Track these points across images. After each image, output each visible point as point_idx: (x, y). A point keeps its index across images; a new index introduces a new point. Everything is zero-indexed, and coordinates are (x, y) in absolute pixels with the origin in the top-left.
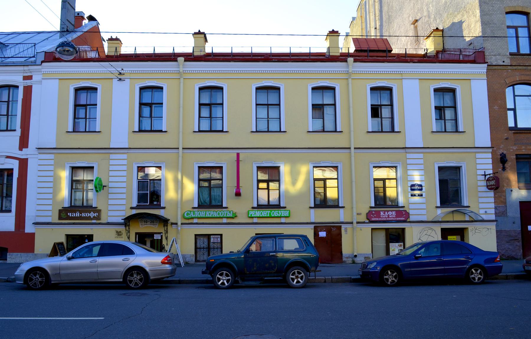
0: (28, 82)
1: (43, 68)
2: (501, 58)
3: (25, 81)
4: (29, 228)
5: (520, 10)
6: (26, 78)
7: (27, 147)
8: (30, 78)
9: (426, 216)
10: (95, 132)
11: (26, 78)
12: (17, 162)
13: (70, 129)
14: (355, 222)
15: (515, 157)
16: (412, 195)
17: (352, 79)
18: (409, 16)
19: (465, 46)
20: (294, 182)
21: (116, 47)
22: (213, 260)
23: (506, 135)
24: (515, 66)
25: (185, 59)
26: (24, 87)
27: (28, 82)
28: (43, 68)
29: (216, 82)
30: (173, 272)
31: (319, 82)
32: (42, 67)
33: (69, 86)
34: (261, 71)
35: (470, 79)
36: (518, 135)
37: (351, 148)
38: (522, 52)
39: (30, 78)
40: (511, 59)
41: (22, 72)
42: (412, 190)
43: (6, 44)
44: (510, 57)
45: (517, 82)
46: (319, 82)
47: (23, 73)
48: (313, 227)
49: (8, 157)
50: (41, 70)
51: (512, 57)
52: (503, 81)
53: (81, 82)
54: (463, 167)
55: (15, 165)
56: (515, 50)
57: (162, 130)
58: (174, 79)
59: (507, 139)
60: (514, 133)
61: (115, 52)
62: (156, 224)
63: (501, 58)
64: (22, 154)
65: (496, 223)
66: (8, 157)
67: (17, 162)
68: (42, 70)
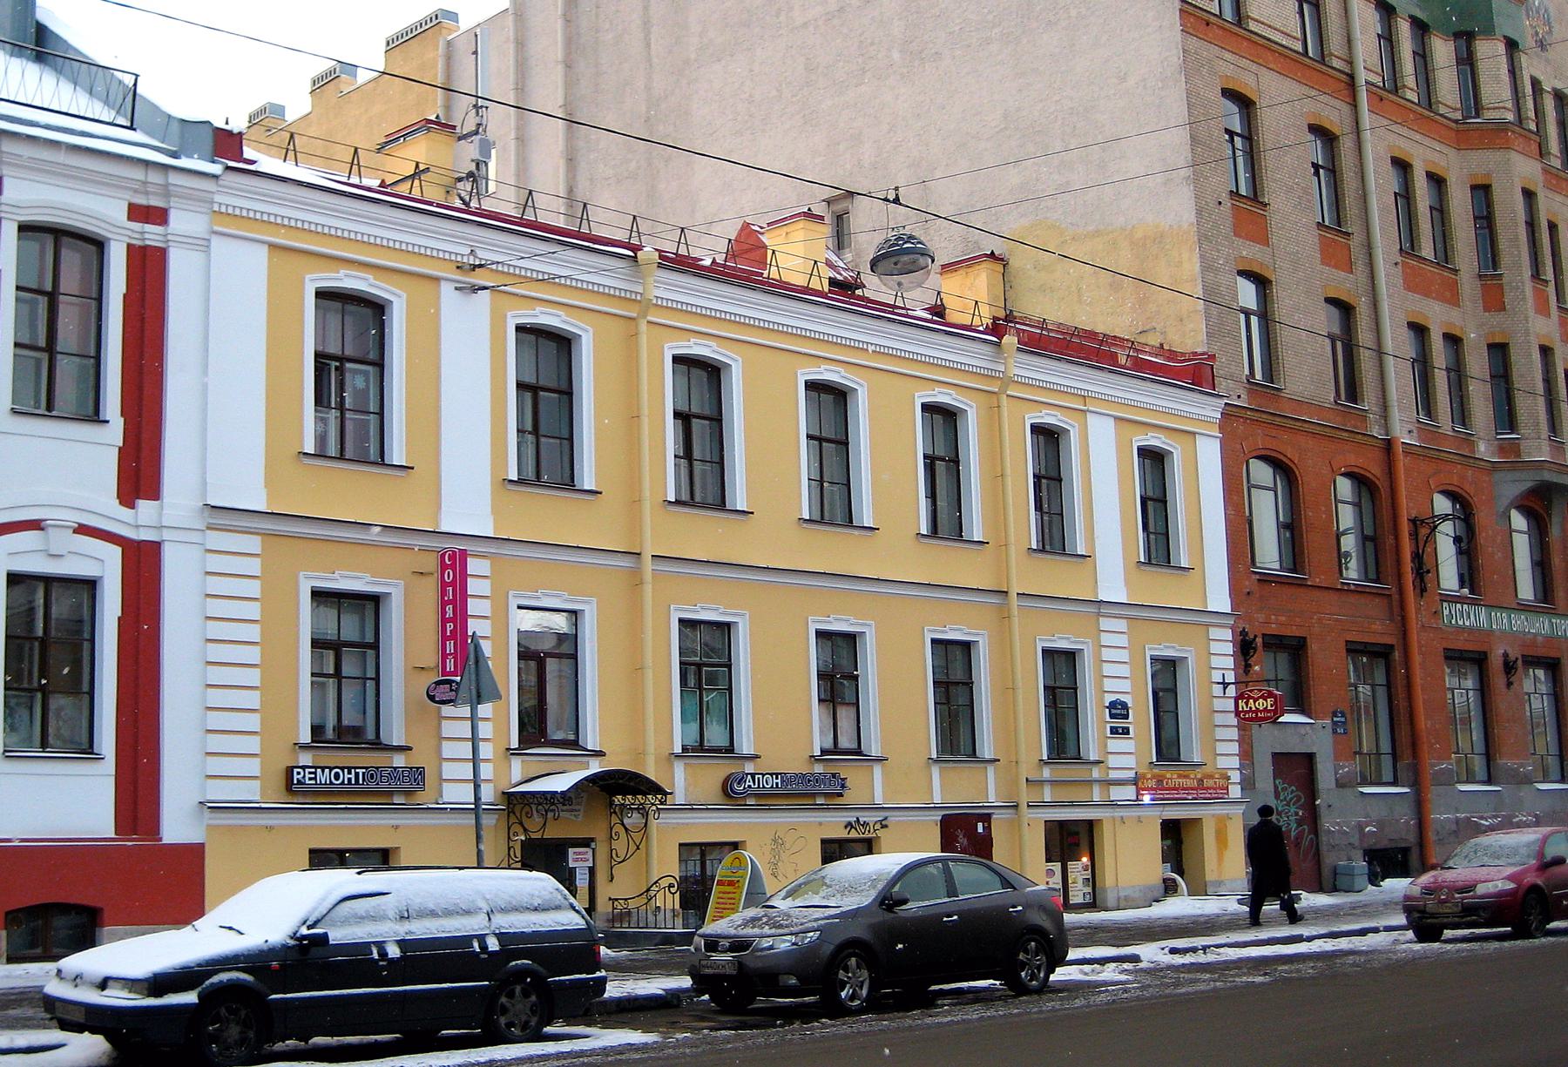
0: (152, 234)
1: (220, 189)
2: (1234, 386)
3: (137, 226)
4: (177, 826)
6: (138, 213)
7: (155, 494)
8: (157, 216)
9: (492, 785)
10: (326, 457)
11: (138, 213)
12: (114, 553)
13: (310, 448)
16: (1114, 731)
17: (648, 322)
21: (356, 149)
22: (955, 917)
26: (129, 246)
27: (152, 234)
28: (220, 189)
29: (843, 373)
31: (691, 343)
32: (220, 186)
33: (506, 315)
34: (330, 227)
35: (1194, 434)
37: (642, 555)
39: (157, 216)
41: (130, 189)
42: (1112, 716)
44: (1247, 386)
46: (691, 343)
47: (131, 193)
48: (940, 818)
49: (83, 530)
50: (210, 195)
51: (1251, 387)
52: (1239, 446)
53: (537, 308)
54: (867, 634)
55: (107, 566)
58: (754, 347)
60: (1258, 580)
61: (352, 163)
62: (577, 807)
63: (1234, 386)
64: (140, 521)
65: (1244, 807)
66: (83, 530)
67: (116, 551)
68: (218, 198)
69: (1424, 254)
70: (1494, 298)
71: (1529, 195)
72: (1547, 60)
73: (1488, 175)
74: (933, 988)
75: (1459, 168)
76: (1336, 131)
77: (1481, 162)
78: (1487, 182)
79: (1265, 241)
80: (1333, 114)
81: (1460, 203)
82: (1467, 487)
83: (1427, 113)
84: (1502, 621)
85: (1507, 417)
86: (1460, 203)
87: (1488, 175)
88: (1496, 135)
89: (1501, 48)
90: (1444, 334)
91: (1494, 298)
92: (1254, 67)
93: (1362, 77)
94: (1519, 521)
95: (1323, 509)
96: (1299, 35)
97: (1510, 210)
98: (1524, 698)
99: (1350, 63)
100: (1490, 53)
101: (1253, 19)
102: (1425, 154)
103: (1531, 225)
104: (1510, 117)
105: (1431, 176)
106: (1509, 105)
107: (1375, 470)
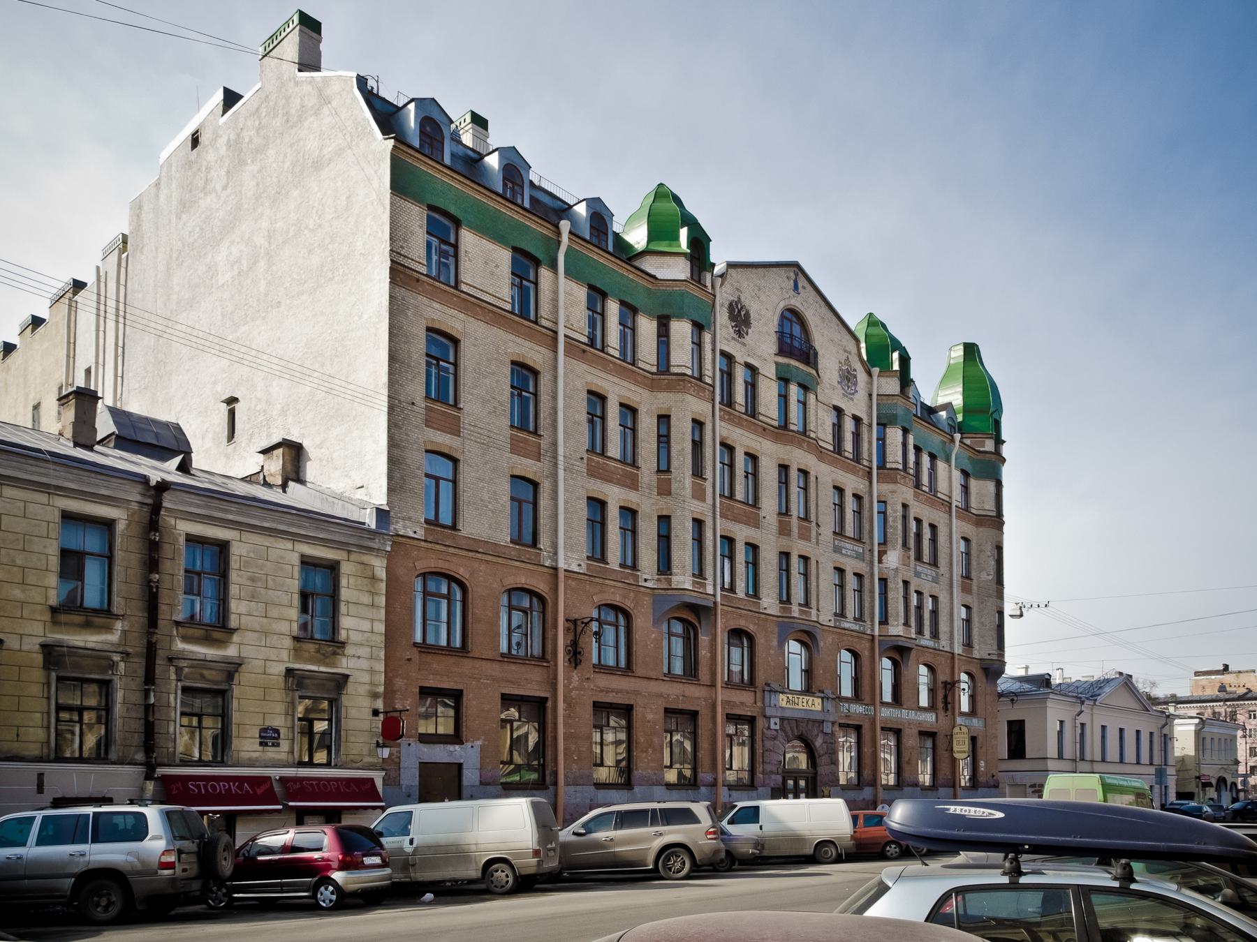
5: (446, 451)
14: (1028, 785)
15: (418, 690)
18: (215, 383)
19: (348, 486)
20: (192, 785)
23: (408, 653)
24: (431, 542)
25: (851, 805)
30: (1246, 694)
36: (424, 655)
38: (441, 521)
40: (426, 530)
43: (1168, 868)
44: (425, 526)
45: (759, 759)
52: (411, 565)
56: (432, 517)
57: (729, 790)
59: (409, 660)
69: (848, 534)
70: (665, 489)
71: (905, 506)
72: (744, 345)
73: (669, 409)
74: (236, 895)
75: (649, 404)
76: (537, 367)
77: (664, 401)
78: (668, 414)
79: (457, 432)
80: (535, 355)
81: (647, 426)
82: (854, 645)
83: (839, 457)
84: (912, 715)
85: (665, 565)
86: (647, 426)
87: (669, 409)
88: (678, 382)
89: (900, 432)
90: (621, 508)
91: (665, 489)
92: (462, 316)
93: (954, 504)
94: (887, 663)
95: (772, 652)
96: (744, 404)
97: (895, 512)
98: (590, 737)
99: (950, 497)
100: (681, 330)
101: (464, 283)
102: (853, 483)
103: (905, 517)
104: (900, 467)
105: (855, 495)
106: (901, 461)
107: (542, 587)
